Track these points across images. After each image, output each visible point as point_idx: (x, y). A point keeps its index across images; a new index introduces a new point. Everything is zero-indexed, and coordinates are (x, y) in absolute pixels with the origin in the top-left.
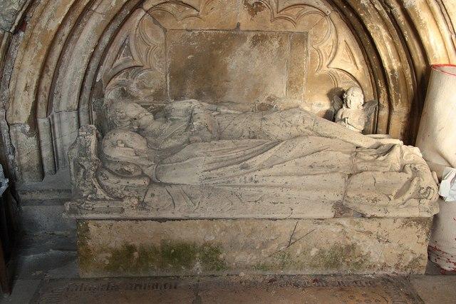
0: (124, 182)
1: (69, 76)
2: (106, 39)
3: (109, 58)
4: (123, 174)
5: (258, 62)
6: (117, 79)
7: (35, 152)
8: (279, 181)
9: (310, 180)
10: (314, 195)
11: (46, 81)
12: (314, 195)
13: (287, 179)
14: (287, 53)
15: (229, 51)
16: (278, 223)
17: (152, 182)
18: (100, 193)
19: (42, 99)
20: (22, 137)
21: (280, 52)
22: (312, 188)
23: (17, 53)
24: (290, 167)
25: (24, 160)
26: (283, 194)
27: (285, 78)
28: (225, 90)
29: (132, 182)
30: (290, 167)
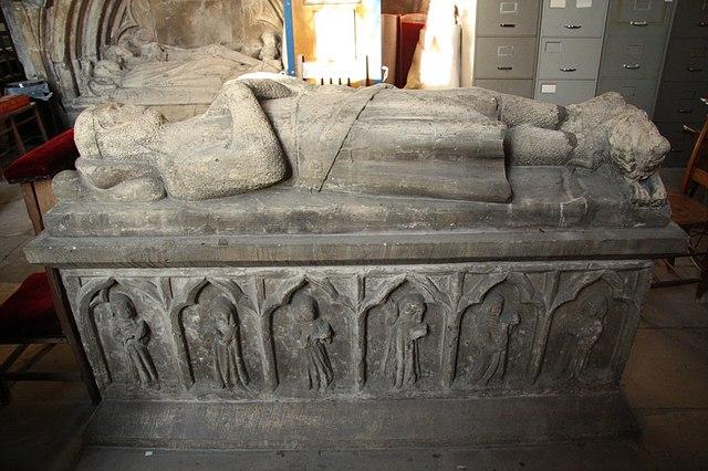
0: (102, 88)
1: (89, 32)
2: (109, 10)
3: (117, 21)
4: (103, 83)
5: (211, 19)
6: (125, 35)
7: (71, 78)
8: (185, 83)
9: (202, 82)
10: (203, 90)
11: (73, 37)
12: (203, 90)
13: (189, 81)
14: (229, 12)
15: (191, 13)
16: (185, 107)
17: (118, 87)
18: (90, 93)
19: (72, 47)
20: (62, 71)
21: (224, 11)
22: (203, 86)
23: (51, 19)
24: (191, 75)
25: (66, 85)
26: (187, 90)
27: (231, 30)
28: (192, 39)
29: (107, 87)
30: (191, 75)
